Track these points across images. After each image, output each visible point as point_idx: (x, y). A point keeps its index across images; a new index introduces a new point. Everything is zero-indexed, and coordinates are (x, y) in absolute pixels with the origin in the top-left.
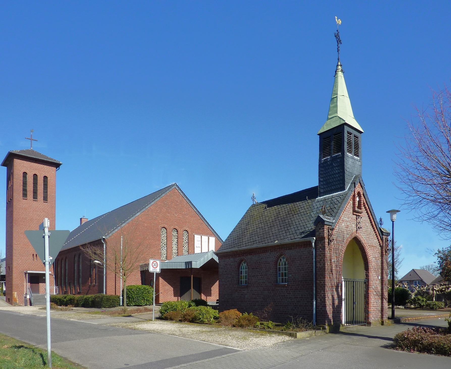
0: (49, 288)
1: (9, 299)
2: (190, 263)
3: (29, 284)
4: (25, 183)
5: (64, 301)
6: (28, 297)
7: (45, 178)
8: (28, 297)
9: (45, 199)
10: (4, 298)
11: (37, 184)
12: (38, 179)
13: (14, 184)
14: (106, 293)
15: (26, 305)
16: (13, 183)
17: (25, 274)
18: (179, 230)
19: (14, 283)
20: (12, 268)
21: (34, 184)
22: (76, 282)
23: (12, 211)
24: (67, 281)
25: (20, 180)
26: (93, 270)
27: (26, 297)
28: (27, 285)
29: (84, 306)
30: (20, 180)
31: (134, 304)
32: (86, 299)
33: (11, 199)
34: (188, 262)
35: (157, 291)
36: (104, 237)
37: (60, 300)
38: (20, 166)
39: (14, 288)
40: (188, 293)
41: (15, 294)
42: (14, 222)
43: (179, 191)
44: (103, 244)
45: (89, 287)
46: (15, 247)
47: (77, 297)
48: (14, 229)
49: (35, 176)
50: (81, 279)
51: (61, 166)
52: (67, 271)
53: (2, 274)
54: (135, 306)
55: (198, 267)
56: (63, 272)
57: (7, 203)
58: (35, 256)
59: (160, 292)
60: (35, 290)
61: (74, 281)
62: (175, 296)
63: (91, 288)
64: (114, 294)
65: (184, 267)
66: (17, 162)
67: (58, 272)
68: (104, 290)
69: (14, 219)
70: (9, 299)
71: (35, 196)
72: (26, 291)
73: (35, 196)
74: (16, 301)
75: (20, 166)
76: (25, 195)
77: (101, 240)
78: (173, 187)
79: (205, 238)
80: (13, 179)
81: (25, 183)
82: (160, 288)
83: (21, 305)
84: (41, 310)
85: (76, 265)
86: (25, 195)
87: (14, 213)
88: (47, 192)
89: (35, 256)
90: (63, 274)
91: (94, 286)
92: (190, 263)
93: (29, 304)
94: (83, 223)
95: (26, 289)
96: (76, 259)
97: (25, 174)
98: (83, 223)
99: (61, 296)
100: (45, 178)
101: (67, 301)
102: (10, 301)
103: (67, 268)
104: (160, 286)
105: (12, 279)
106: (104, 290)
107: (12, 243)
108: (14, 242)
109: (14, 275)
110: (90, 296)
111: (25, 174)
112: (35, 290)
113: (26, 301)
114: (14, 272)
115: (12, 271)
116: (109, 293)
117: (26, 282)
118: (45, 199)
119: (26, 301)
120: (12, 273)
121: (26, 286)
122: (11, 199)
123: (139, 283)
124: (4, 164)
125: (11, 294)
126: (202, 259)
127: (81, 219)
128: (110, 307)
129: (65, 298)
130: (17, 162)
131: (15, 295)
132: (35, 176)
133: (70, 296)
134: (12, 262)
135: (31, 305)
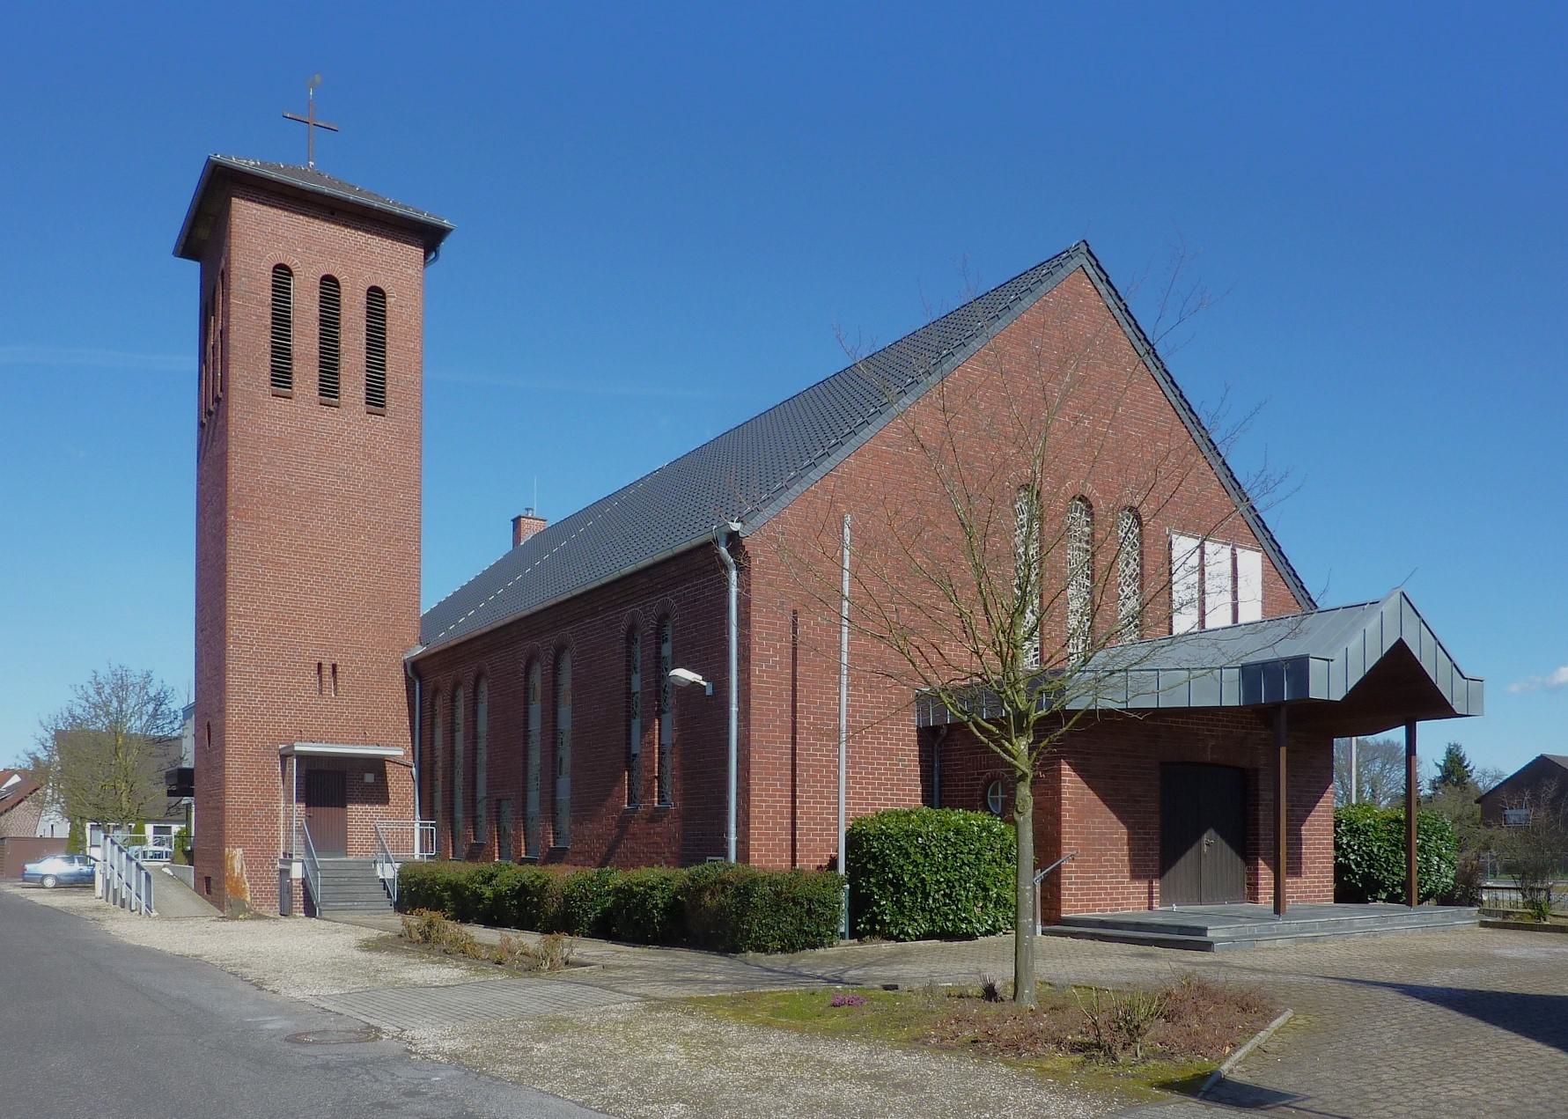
0: (393, 836)
1: (208, 879)
2: (1299, 667)
3: (299, 809)
4: (281, 321)
5: (479, 898)
6: (297, 871)
7: (376, 296)
8: (297, 871)
9: (376, 396)
10: (189, 872)
11: (336, 325)
12: (344, 299)
13: (233, 329)
14: (743, 855)
15: (286, 913)
16: (226, 315)
17: (284, 758)
18: (1101, 506)
19: (229, 805)
20: (222, 733)
21: (323, 322)
22: (534, 796)
23: (224, 455)
24: (482, 792)
25: (261, 303)
26: (646, 728)
27: (285, 873)
28: (290, 813)
29: (604, 929)
30: (261, 303)
31: (925, 927)
32: (624, 893)
33: (217, 400)
34: (1264, 666)
35: (1048, 846)
36: (736, 526)
37: (455, 889)
38: (258, 232)
39: (230, 826)
40: (1191, 854)
41: (236, 858)
42: (232, 503)
43: (1102, 287)
44: (725, 567)
45: (624, 821)
46: (234, 626)
47: (561, 876)
48: (230, 539)
49: (329, 283)
50: (564, 783)
51: (444, 246)
52: (483, 744)
53: (185, 765)
54: (928, 936)
55: (1338, 695)
56: (460, 747)
57: (201, 425)
58: (327, 671)
59: (1066, 851)
60: (327, 839)
61: (525, 790)
62: (1135, 876)
63: (634, 828)
64: (786, 864)
65: (1232, 697)
66: (246, 215)
67: (432, 748)
68: (733, 839)
69: (232, 491)
70: (208, 879)
71: (329, 386)
72: (288, 843)
73: (329, 386)
74: (238, 891)
75: (258, 232)
76: (282, 375)
77: (708, 547)
78: (1072, 265)
79: (1218, 555)
80: (226, 301)
81: (281, 321)
82: (1066, 828)
83: (264, 910)
84: (380, 959)
85: (536, 709)
86: (282, 375)
87: (231, 463)
88: (382, 367)
89: (327, 671)
90: (460, 760)
91: (655, 817)
92: (1299, 667)
93: (299, 904)
94: (527, 536)
95: (289, 831)
96: (537, 679)
97: (282, 273)
98: (527, 536)
99: (460, 871)
100: (376, 296)
101: (498, 897)
102: (212, 887)
103: (483, 727)
104: (1066, 817)
105: (220, 785)
106: (733, 839)
107: (223, 607)
108: (233, 602)
109: (234, 765)
110: (658, 876)
111: (282, 273)
112: (327, 839)
113: (285, 891)
114: (230, 749)
115: (223, 744)
116: (768, 856)
117: (289, 801)
118: (376, 396)
119: (285, 891)
120: (222, 755)
121: (288, 817)
122: (217, 400)
123: (911, 796)
124: (189, 247)
125: (220, 861)
126: (1354, 644)
127: (517, 522)
128: (790, 947)
129: (488, 879)
130: (246, 215)
131: (237, 865)
132: (329, 283)
133: (511, 874)
134: (222, 701)
135: (310, 911)
